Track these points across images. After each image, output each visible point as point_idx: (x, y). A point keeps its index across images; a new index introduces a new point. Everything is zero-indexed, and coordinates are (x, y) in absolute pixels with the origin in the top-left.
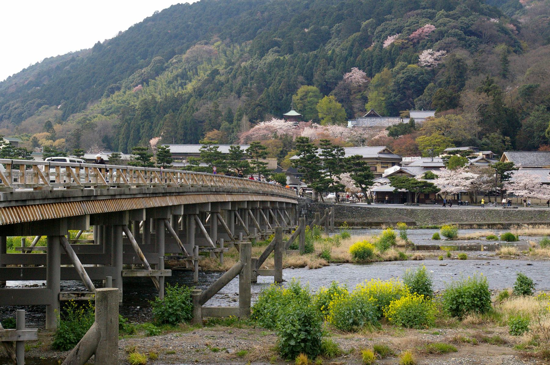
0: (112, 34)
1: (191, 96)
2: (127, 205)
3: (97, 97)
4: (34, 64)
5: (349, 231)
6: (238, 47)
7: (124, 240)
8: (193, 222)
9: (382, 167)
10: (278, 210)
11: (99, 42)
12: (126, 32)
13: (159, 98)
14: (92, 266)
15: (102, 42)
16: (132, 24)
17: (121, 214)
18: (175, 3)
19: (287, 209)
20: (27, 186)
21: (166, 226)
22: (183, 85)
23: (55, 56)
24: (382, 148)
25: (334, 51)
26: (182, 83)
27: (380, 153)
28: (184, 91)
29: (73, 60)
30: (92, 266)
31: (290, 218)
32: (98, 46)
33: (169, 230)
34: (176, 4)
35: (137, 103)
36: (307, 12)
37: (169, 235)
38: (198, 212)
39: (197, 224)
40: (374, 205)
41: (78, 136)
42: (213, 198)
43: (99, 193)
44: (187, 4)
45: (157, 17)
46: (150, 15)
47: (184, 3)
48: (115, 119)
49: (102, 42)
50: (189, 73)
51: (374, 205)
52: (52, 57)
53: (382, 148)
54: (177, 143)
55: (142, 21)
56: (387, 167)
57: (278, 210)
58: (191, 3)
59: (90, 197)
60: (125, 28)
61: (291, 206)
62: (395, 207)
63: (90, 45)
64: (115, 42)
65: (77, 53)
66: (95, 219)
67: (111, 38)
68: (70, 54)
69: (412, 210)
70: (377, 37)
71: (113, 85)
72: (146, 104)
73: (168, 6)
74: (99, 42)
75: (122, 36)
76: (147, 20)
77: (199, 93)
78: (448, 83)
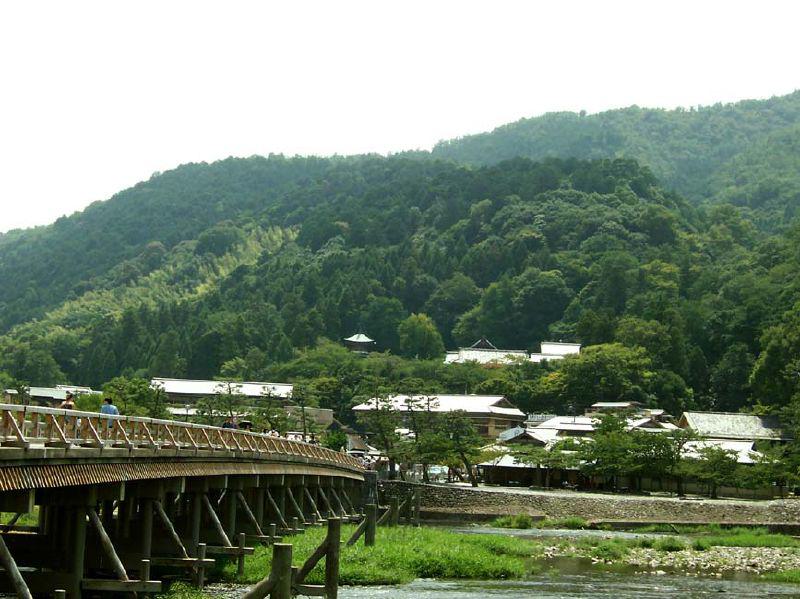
1: (200, 305)
2: (95, 478)
3: (56, 301)
6: (280, 232)
7: (88, 528)
8: (198, 501)
9: (496, 428)
10: (333, 491)
12: (109, 202)
13: (153, 306)
14: (32, 569)
15: (68, 216)
17: (85, 489)
18: (185, 162)
19: (346, 488)
20: (43, 401)
21: (155, 508)
22: (190, 288)
23: (289, 154)
24: (498, 398)
25: (426, 248)
26: (189, 284)
28: (192, 296)
29: (22, 241)
30: (32, 569)
31: (350, 502)
32: (62, 223)
33: (159, 514)
34: (187, 162)
35: (118, 314)
36: (385, 185)
37: (159, 524)
38: (207, 490)
39: (205, 509)
42: (231, 470)
43: (52, 455)
45: (157, 181)
46: (146, 178)
49: (68, 216)
50: (201, 268)
51: (482, 488)
52: (76, 213)
53: (498, 398)
54: (177, 376)
56: (505, 429)
57: (333, 491)
59: (38, 460)
60: (105, 194)
61: (353, 485)
63: (48, 220)
65: (29, 230)
66: (42, 495)
72: (130, 314)
75: (96, 211)
77: (213, 302)
78: (600, 302)
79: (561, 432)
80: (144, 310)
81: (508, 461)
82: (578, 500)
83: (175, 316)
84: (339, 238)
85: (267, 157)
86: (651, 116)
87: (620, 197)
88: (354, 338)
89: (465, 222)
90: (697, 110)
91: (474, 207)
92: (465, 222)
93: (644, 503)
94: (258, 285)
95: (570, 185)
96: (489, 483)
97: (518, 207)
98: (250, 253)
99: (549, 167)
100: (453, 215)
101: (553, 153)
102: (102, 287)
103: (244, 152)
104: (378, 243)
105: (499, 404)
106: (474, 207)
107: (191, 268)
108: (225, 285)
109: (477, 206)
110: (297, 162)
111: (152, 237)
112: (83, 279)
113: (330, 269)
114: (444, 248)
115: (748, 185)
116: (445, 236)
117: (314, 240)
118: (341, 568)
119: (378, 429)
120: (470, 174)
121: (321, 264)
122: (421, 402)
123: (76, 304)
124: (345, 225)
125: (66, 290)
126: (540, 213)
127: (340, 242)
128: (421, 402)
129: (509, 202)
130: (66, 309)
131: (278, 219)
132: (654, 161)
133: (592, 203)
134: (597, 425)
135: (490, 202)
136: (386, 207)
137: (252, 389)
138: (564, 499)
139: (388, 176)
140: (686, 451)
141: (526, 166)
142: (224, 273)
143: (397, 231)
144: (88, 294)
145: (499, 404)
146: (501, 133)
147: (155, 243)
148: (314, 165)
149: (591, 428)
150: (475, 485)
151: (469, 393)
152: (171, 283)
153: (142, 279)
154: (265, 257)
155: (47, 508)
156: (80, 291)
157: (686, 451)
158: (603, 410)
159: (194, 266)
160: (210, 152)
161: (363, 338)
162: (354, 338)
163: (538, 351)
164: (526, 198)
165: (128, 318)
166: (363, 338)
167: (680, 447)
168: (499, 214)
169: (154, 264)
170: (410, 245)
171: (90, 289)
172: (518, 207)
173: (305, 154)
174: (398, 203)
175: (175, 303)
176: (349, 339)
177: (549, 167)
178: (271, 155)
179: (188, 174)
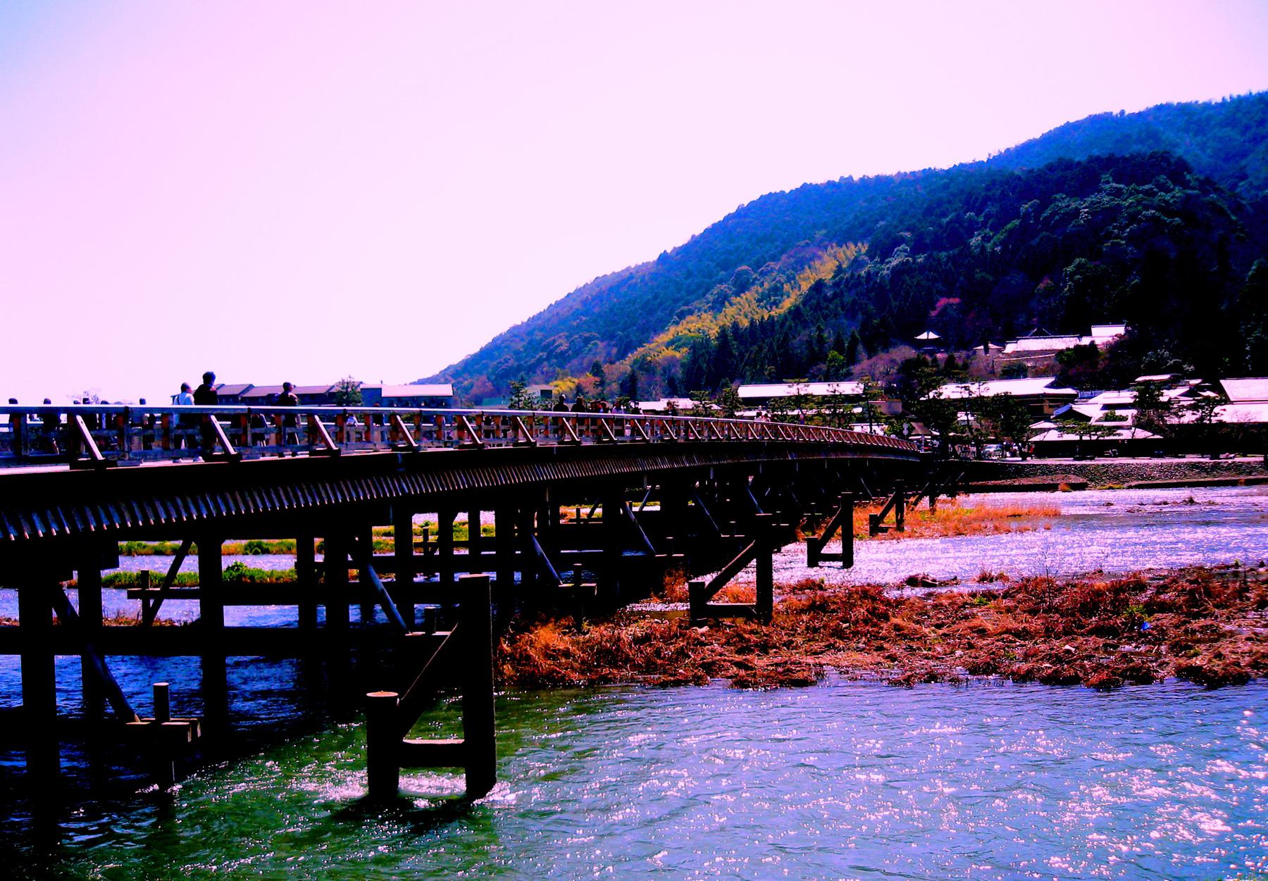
0: (682, 239)
3: (660, 327)
4: (581, 285)
5: (1148, 566)
9: (1050, 407)
11: (665, 251)
15: (669, 251)
16: (708, 224)
18: (765, 192)
24: (1050, 380)
27: (1047, 387)
29: (611, 289)
32: (664, 258)
35: (714, 332)
40: (1031, 461)
41: (633, 378)
44: (782, 193)
46: (733, 210)
47: (778, 191)
48: (682, 354)
49: (669, 251)
50: (785, 286)
51: (1031, 461)
53: (1050, 380)
55: (722, 219)
58: (787, 191)
60: (698, 231)
62: (1058, 463)
63: (653, 257)
64: (685, 250)
67: (680, 245)
68: (628, 269)
69: (1082, 466)
70: (124, 861)
71: (685, 308)
73: (755, 197)
74: (665, 251)
75: (695, 241)
76: (729, 218)
79: (1106, 407)
80: (735, 326)
81: (1053, 436)
82: (1116, 466)
83: (762, 330)
84: (903, 246)
85: (837, 180)
86: (1185, 110)
87: (1157, 186)
88: (924, 336)
89: (1017, 222)
90: (1229, 100)
91: (1024, 207)
92: (1017, 222)
93: (1178, 465)
94: (835, 295)
95: (1111, 179)
96: (1039, 456)
97: (1064, 202)
98: (825, 269)
99: (1092, 164)
100: (1009, 213)
101: (1096, 152)
102: (699, 310)
103: (819, 177)
104: (942, 248)
105: (1051, 386)
106: (1024, 207)
107: (776, 286)
108: (807, 300)
109: (1027, 206)
110: (864, 181)
111: (741, 261)
112: (684, 305)
113: (897, 272)
114: (1000, 248)
115: (1250, 179)
116: (1000, 236)
117: (883, 250)
118: (806, 547)
119: (942, 413)
120: (1019, 178)
121: (888, 272)
122: (977, 389)
123: (680, 328)
124: (908, 235)
125: (670, 315)
126: (1084, 208)
127: (905, 251)
128: (977, 389)
129: (1056, 199)
130: (664, 337)
131: (844, 238)
132: (1185, 147)
133: (1131, 194)
134: (1135, 397)
135: (1038, 201)
136: (944, 215)
137: (819, 389)
138: (1103, 465)
139: (946, 187)
140: (1216, 415)
141: (1069, 165)
142: (805, 287)
143: (956, 235)
144: (689, 318)
145: (1051, 386)
146: (1049, 139)
147: (744, 267)
148: (881, 184)
149: (1132, 401)
150: (1024, 459)
151: (1025, 377)
152: (759, 301)
153: (735, 300)
154: (839, 270)
155: (1034, 426)
156: (682, 316)
157: (1216, 415)
158: (1140, 383)
159: (779, 285)
160: (788, 183)
161: (932, 336)
162: (924, 336)
163: (1089, 334)
164: (1071, 194)
165: (723, 335)
166: (932, 336)
167: (1211, 411)
168: (1047, 213)
169: (742, 288)
170: (969, 247)
171: (691, 313)
172: (1064, 202)
173: (871, 173)
174: (956, 210)
175: (763, 318)
176: (919, 337)
177: (1092, 164)
178: (842, 178)
179: (768, 203)
